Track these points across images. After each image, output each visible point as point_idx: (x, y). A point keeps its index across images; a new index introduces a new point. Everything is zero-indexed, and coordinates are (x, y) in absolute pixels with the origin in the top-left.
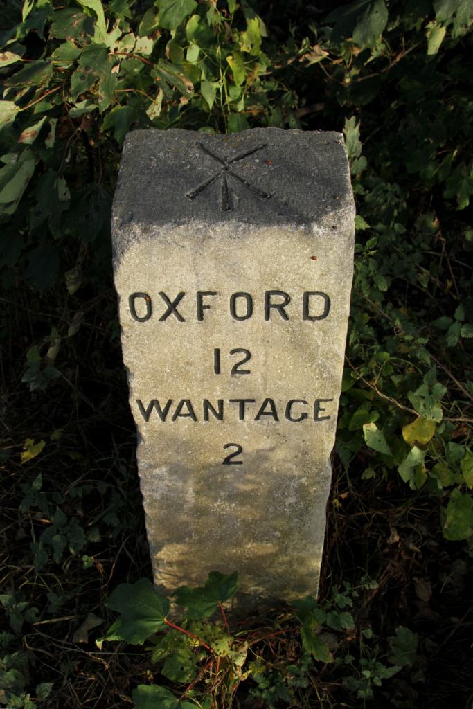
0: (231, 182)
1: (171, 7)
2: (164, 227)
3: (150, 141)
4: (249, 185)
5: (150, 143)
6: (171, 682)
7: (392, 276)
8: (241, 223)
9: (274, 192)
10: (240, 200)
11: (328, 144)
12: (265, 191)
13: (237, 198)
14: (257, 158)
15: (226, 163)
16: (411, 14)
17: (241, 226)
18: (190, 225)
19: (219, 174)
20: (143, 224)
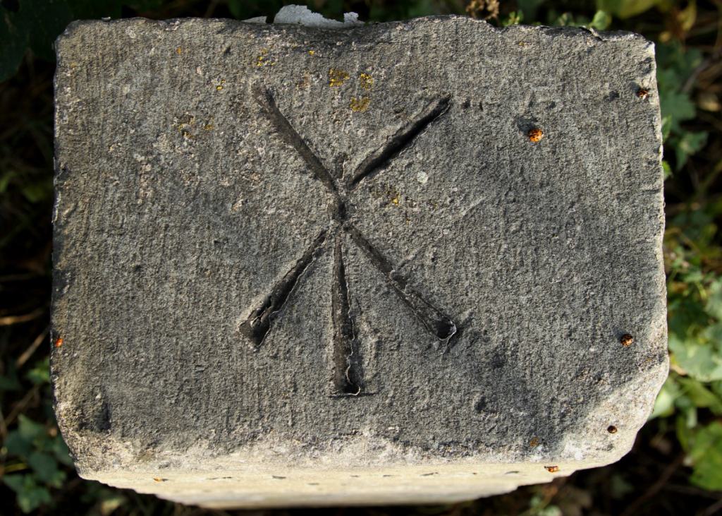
0: (358, 261)
1: (349, 331)
2: (193, 450)
3: (128, 79)
4: (402, 281)
5: (127, 89)
6: (305, 159)
7: (275, 25)
8: (383, 442)
9: (467, 313)
10: (379, 344)
11: (615, 95)
12: (445, 304)
13: (371, 341)
14: (424, 166)
15: (339, 183)
16: (60, 344)
17: (384, 448)
18: (256, 448)
19: (322, 237)
20: (138, 442)
